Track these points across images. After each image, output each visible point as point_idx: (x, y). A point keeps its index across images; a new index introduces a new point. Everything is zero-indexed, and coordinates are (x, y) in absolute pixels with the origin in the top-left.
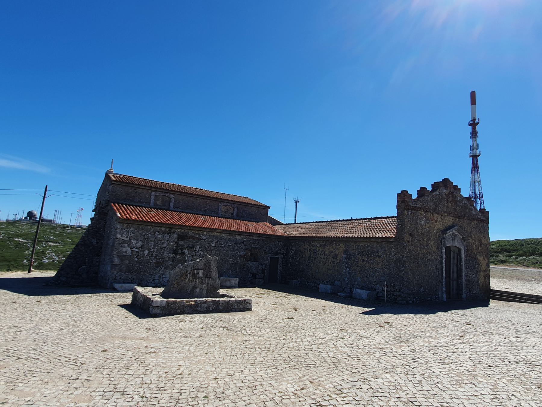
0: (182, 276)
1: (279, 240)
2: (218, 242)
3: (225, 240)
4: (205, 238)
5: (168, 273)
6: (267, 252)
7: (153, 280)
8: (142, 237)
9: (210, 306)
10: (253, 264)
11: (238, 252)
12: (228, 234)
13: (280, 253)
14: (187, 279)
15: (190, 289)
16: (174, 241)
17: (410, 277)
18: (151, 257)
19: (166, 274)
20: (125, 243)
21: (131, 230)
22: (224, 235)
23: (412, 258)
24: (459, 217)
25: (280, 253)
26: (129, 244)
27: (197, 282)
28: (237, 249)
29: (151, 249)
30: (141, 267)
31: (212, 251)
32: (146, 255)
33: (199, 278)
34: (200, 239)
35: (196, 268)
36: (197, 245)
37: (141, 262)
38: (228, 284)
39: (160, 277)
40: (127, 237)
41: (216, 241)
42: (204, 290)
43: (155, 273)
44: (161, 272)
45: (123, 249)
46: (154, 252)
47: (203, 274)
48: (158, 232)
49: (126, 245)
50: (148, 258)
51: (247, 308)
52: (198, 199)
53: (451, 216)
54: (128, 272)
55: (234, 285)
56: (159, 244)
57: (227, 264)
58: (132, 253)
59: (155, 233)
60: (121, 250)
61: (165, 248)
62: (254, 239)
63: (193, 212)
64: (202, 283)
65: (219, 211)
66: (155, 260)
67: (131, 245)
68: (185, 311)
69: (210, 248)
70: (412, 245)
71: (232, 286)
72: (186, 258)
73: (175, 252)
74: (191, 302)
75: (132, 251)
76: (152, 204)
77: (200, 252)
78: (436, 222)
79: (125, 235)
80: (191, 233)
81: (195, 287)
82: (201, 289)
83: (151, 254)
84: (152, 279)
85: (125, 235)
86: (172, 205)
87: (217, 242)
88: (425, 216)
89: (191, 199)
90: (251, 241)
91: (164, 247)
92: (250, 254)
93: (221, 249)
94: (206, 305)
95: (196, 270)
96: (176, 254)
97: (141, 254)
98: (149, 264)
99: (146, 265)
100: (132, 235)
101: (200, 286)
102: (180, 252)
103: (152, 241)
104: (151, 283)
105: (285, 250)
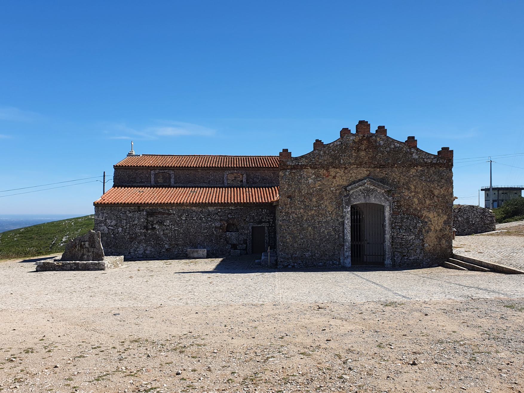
0: (72, 247)
1: (262, 207)
2: (189, 216)
3: (197, 213)
4: (174, 212)
8: (115, 216)
10: (231, 234)
11: (212, 224)
13: (264, 222)
16: (144, 218)
17: (288, 240)
18: (125, 233)
19: (140, 247)
22: (194, 208)
24: (381, 167)
25: (264, 222)
28: (210, 221)
29: (124, 227)
33: (85, 248)
35: (83, 240)
36: (167, 220)
38: (195, 255)
39: (135, 250)
40: (102, 218)
46: (127, 228)
47: (89, 244)
48: (129, 211)
49: (103, 224)
50: (122, 234)
53: (364, 167)
54: (107, 247)
55: (202, 256)
57: (201, 236)
58: (108, 231)
59: (126, 212)
61: (136, 224)
64: (89, 252)
69: (180, 221)
72: (158, 233)
73: (146, 228)
75: (108, 229)
81: (83, 255)
82: (88, 256)
83: (124, 231)
86: (172, 180)
88: (314, 174)
90: (226, 212)
91: (135, 224)
92: (226, 225)
94: (69, 266)
96: (147, 230)
97: (116, 231)
102: (151, 227)
103: (124, 219)
104: (128, 255)
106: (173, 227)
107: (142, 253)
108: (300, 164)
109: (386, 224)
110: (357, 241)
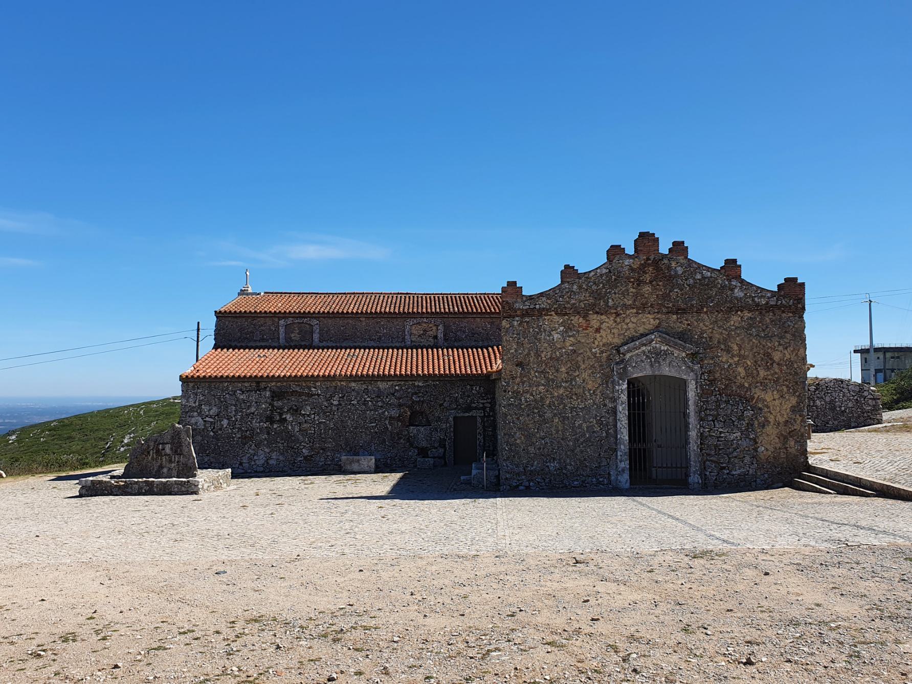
0: (143, 454)
1: (472, 383)
4: (319, 391)
6: (446, 408)
8: (216, 400)
12: (362, 382)
16: (266, 402)
18: (233, 428)
20: (194, 411)
23: (523, 406)
25: (476, 408)
26: (199, 411)
28: (381, 406)
29: (232, 417)
31: (334, 413)
32: (225, 426)
36: (307, 405)
38: (355, 467)
40: (195, 403)
41: (340, 395)
46: (237, 421)
47: (171, 449)
49: (196, 414)
52: (361, 319)
55: (367, 469)
58: (205, 425)
61: (253, 413)
63: (355, 344)
64: (171, 461)
65: (405, 335)
67: (203, 413)
73: (270, 419)
75: (205, 421)
76: (282, 341)
77: (313, 416)
78: (598, 330)
80: (294, 387)
81: (161, 467)
82: (169, 469)
83: (232, 425)
84: (238, 463)
86: (316, 337)
87: (343, 397)
89: (351, 322)
92: (409, 413)
93: (351, 409)
94: (137, 486)
95: (161, 446)
96: (272, 423)
100: (201, 399)
101: (168, 465)
103: (231, 405)
105: (489, 401)
107: (263, 464)
108: (537, 306)
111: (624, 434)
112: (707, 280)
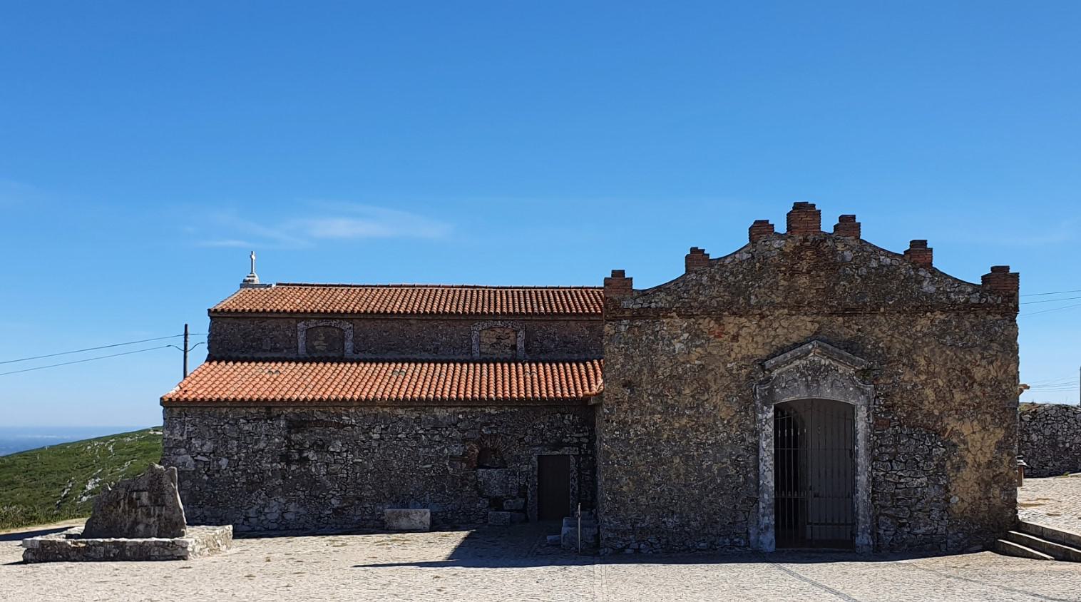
0: (110, 504)
3: (407, 423)
4: (354, 421)
5: (275, 503)
7: (247, 519)
8: (211, 431)
9: (110, 551)
12: (413, 409)
14: (121, 508)
15: (127, 525)
16: (280, 435)
18: (235, 470)
20: (180, 447)
21: (189, 419)
22: (400, 411)
24: (848, 312)
25: (568, 444)
26: (187, 447)
27: (140, 513)
28: (440, 442)
29: (233, 456)
30: (216, 492)
31: (374, 450)
34: (341, 426)
35: (136, 488)
36: (336, 439)
37: (215, 482)
38: (404, 523)
39: (259, 512)
40: (182, 435)
42: (153, 527)
43: (247, 505)
44: (259, 501)
45: (177, 459)
46: (240, 460)
47: (150, 498)
48: (245, 418)
49: (183, 450)
51: (178, 555)
55: (420, 526)
56: (249, 444)
58: (195, 466)
59: (237, 421)
60: (173, 461)
61: (263, 450)
62: (485, 415)
63: (402, 356)
64: (149, 515)
66: (244, 476)
67: (193, 449)
68: (69, 556)
69: (368, 443)
70: (632, 411)
71: (413, 528)
72: (313, 470)
73: (286, 458)
74: (79, 544)
75: (196, 460)
79: (177, 431)
81: (136, 523)
83: (234, 465)
85: (177, 431)
86: (349, 345)
89: (396, 325)
90: (478, 420)
94: (102, 549)
96: (289, 463)
97: (214, 466)
98: (233, 486)
99: (227, 487)
102: (297, 457)
106: (350, 456)
107: (277, 520)
109: (857, 450)
110: (789, 489)
111: (769, 479)
112: (885, 269)
